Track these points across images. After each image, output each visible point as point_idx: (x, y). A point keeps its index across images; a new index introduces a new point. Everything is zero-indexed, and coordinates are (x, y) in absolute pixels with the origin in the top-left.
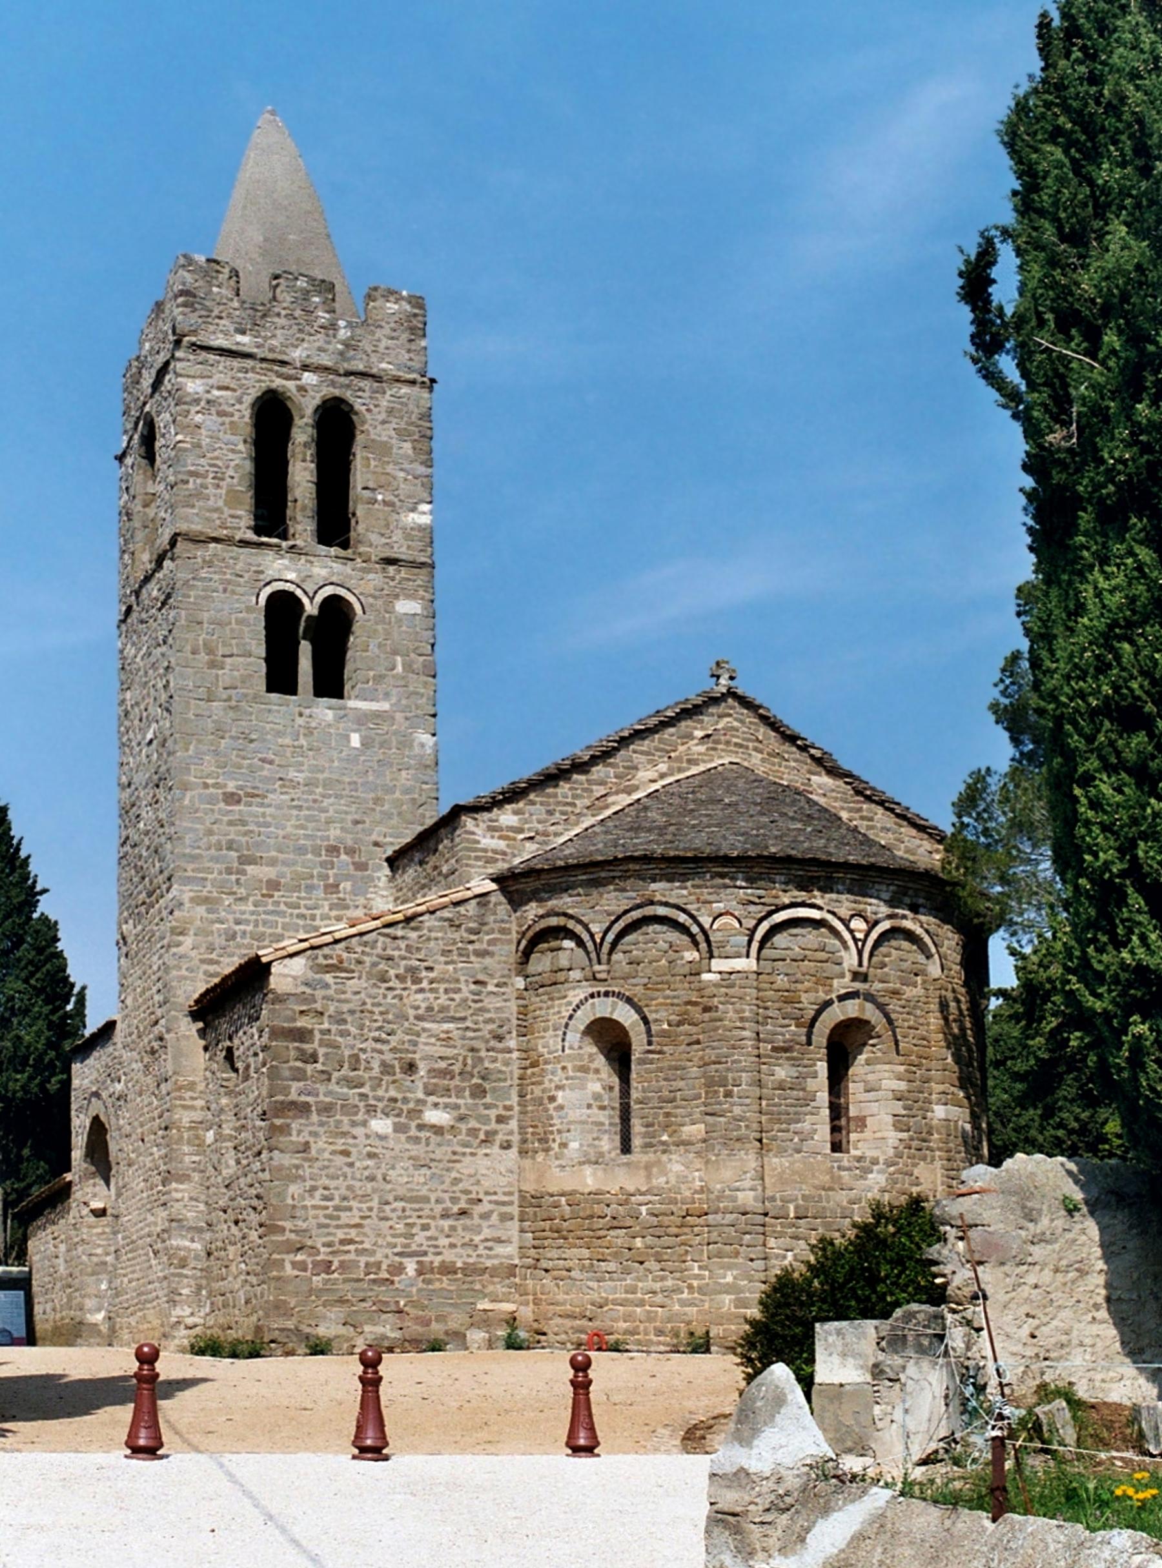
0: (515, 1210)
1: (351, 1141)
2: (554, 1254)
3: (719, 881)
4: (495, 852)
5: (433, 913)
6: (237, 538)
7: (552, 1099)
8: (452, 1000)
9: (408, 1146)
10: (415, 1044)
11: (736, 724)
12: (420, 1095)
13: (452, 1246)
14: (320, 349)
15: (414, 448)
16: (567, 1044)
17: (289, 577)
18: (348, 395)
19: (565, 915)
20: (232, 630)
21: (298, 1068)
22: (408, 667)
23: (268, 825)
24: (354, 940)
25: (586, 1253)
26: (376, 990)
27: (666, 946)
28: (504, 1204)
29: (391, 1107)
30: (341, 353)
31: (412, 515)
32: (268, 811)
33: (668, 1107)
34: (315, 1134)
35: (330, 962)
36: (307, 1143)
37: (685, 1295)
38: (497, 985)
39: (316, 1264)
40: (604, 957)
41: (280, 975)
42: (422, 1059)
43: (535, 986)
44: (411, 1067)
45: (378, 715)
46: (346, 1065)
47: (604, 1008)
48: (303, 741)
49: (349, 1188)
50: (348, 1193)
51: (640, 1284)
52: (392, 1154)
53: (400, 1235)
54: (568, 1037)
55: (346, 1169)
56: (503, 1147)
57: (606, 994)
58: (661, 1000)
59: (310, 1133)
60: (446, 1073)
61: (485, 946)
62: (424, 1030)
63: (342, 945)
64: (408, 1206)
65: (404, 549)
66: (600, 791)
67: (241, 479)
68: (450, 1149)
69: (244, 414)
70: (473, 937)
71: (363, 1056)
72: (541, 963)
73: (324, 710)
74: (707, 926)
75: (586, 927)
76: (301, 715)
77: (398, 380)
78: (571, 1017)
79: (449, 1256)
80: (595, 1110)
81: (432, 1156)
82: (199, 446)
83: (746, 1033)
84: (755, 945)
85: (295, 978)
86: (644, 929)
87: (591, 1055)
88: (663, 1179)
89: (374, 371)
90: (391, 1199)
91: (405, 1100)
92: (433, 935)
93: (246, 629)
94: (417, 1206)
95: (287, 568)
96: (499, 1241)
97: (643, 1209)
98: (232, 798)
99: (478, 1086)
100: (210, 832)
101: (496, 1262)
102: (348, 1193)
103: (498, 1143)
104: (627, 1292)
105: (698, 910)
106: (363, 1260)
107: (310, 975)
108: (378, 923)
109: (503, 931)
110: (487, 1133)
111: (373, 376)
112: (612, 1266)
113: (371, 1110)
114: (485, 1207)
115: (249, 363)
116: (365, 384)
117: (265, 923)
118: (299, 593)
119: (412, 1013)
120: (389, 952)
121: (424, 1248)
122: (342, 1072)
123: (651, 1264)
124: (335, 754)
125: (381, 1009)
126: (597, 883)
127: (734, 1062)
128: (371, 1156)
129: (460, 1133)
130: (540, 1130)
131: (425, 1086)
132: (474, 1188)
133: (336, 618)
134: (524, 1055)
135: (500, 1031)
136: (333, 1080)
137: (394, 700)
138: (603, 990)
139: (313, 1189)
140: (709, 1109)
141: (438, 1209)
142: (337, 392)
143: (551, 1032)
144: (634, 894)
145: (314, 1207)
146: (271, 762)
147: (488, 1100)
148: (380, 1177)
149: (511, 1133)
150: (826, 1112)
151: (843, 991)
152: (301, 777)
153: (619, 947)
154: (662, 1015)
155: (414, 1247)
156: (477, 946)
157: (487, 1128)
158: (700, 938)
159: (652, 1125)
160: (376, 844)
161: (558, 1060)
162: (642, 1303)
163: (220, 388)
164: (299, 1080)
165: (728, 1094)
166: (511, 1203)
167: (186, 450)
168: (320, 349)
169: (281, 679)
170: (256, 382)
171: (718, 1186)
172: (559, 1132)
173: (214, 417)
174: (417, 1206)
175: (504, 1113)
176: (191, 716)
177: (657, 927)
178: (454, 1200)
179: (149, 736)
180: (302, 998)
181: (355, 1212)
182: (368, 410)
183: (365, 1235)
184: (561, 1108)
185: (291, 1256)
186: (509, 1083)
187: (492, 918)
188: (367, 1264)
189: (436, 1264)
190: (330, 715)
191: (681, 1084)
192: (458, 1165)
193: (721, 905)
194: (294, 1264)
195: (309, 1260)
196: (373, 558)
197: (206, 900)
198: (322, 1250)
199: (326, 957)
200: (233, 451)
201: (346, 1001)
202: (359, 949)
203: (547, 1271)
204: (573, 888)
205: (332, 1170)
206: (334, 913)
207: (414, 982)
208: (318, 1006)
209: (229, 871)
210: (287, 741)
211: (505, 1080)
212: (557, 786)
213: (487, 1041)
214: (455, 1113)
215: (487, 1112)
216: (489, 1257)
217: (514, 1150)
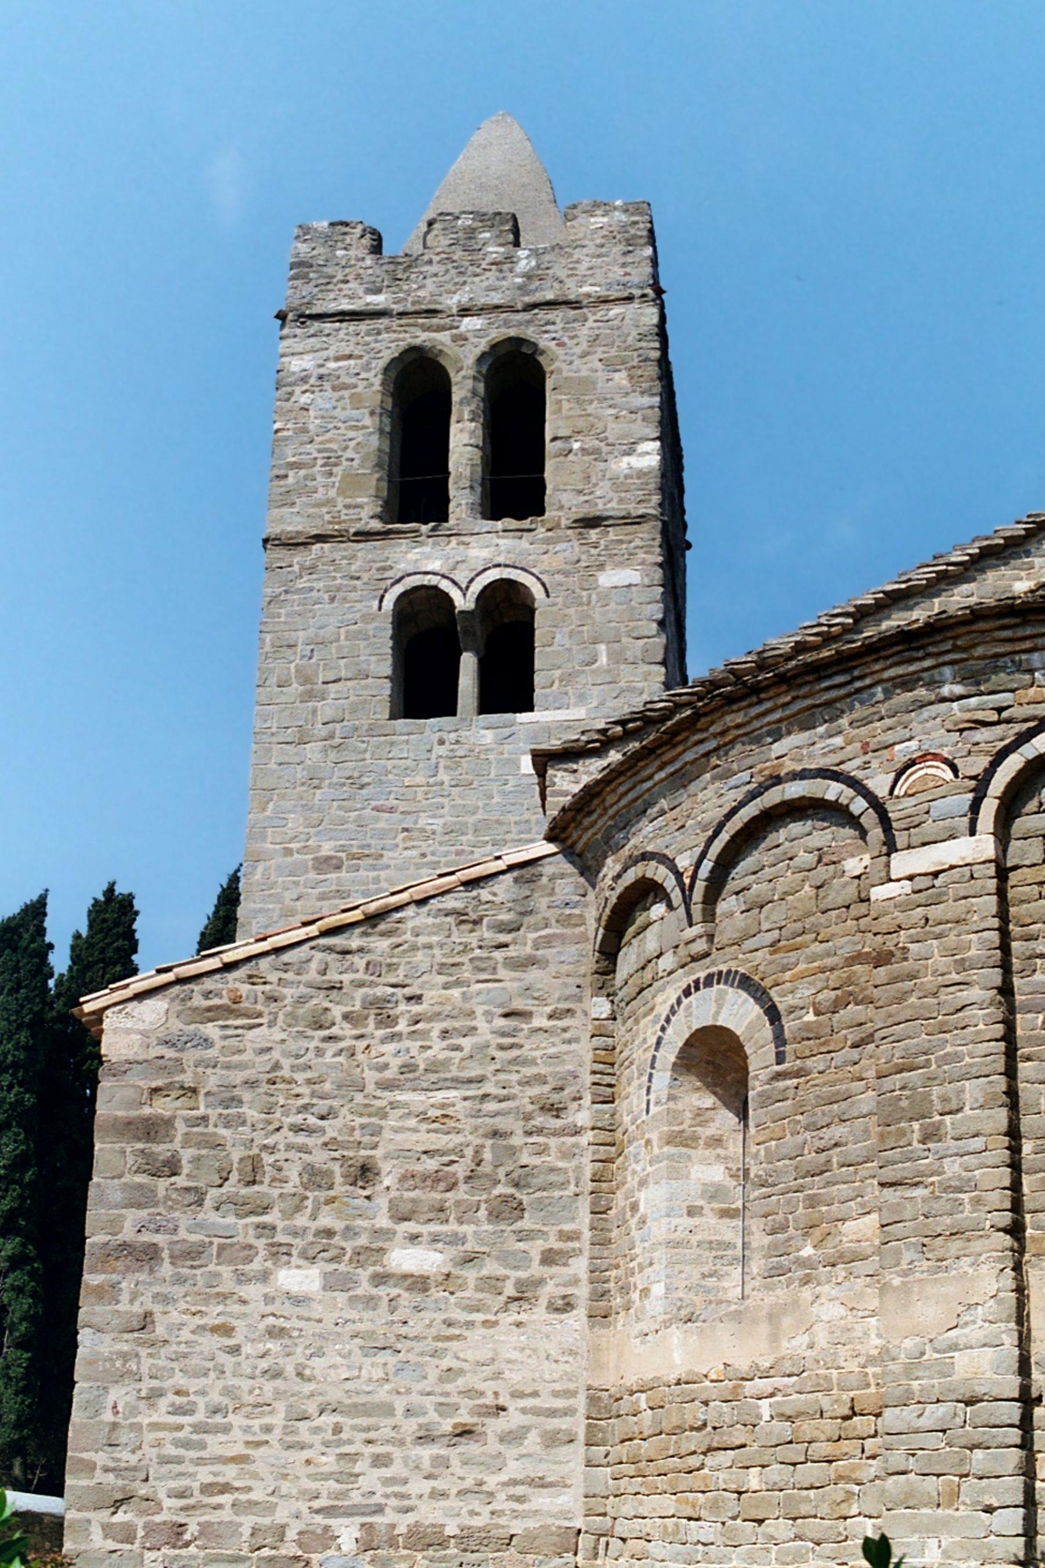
0: (578, 1425)
1: (237, 1308)
3: (905, 697)
5: (422, 902)
6: (352, 531)
8: (458, 1048)
9: (354, 1315)
10: (377, 1131)
12: (383, 1221)
13: (439, 1495)
14: (490, 289)
15: (631, 377)
17: (429, 568)
18: (530, 333)
20: (340, 648)
21: (141, 1186)
22: (618, 658)
24: (264, 963)
25: (668, 1504)
26: (304, 1044)
28: (553, 1413)
29: (322, 1246)
30: (520, 288)
31: (626, 459)
32: (383, 874)
33: (815, 1186)
34: (165, 1299)
35: (216, 1001)
36: (148, 1315)
39: (150, 1529)
40: (697, 916)
41: (115, 1030)
42: (386, 1157)
46: (234, 1177)
48: (443, 776)
49: (227, 1391)
50: (225, 1401)
52: (318, 1328)
53: (326, 1477)
55: (224, 1358)
56: (554, 1308)
57: (709, 981)
58: (802, 966)
59: (156, 1296)
61: (528, 950)
63: (242, 972)
65: (613, 504)
67: (363, 460)
68: (440, 1316)
69: (371, 384)
70: (503, 938)
71: (268, 1159)
76: (442, 742)
79: (428, 1514)
80: (709, 1220)
81: (404, 1330)
82: (305, 430)
84: (989, 807)
85: (144, 1034)
86: (772, 838)
87: (699, 1112)
88: (805, 1339)
89: (572, 297)
90: (312, 1408)
91: (349, 1232)
92: (422, 940)
93: (362, 644)
94: (364, 1421)
95: (428, 557)
97: (765, 1408)
98: (328, 864)
99: (505, 1199)
101: (531, 1524)
102: (225, 1401)
103: (543, 1302)
105: (865, 766)
106: (247, 1522)
107: (176, 1025)
108: (313, 930)
109: (564, 921)
110: (520, 1284)
111: (566, 303)
113: (279, 1253)
114: (513, 1419)
115: (382, 323)
116: (557, 315)
118: (445, 585)
119: (371, 1077)
120: (333, 976)
121: (377, 1499)
122: (227, 1188)
123: (781, 1528)
124: (494, 787)
125: (309, 1074)
127: (946, 1059)
128: (273, 1333)
129: (462, 1287)
131: (392, 1205)
132: (489, 1387)
134: (605, 1137)
135: (555, 1097)
136: (208, 1203)
138: (702, 975)
139: (154, 1395)
140: (889, 1174)
141: (410, 1427)
142: (512, 332)
144: (745, 776)
145: (155, 1426)
146: (392, 810)
147: (527, 1223)
148: (290, 1370)
149: (575, 1282)
152: (438, 824)
155: (356, 1498)
156: (512, 952)
157: (522, 1274)
158: (870, 819)
159: (784, 1228)
163: (337, 359)
164: (139, 1206)
167: (286, 438)
170: (391, 342)
171: (908, 1343)
173: (329, 393)
174: (364, 1421)
175: (557, 1245)
176: (272, 766)
177: (796, 828)
178: (443, 1409)
180: (159, 1065)
181: (236, 1434)
182: (561, 344)
183: (255, 1476)
185: (104, 1515)
187: (544, 902)
189: (402, 1529)
191: (838, 1131)
192: (454, 1345)
193: (913, 744)
194: (108, 1530)
195: (140, 1522)
196: (564, 522)
198: (167, 1502)
200: (355, 428)
201: (241, 1066)
202: (273, 977)
204: (651, 804)
205: (194, 1361)
207: (379, 1024)
208: (187, 1078)
210: (420, 779)
211: (563, 1185)
213: (528, 1117)
214: (454, 1251)
216: (516, 1515)
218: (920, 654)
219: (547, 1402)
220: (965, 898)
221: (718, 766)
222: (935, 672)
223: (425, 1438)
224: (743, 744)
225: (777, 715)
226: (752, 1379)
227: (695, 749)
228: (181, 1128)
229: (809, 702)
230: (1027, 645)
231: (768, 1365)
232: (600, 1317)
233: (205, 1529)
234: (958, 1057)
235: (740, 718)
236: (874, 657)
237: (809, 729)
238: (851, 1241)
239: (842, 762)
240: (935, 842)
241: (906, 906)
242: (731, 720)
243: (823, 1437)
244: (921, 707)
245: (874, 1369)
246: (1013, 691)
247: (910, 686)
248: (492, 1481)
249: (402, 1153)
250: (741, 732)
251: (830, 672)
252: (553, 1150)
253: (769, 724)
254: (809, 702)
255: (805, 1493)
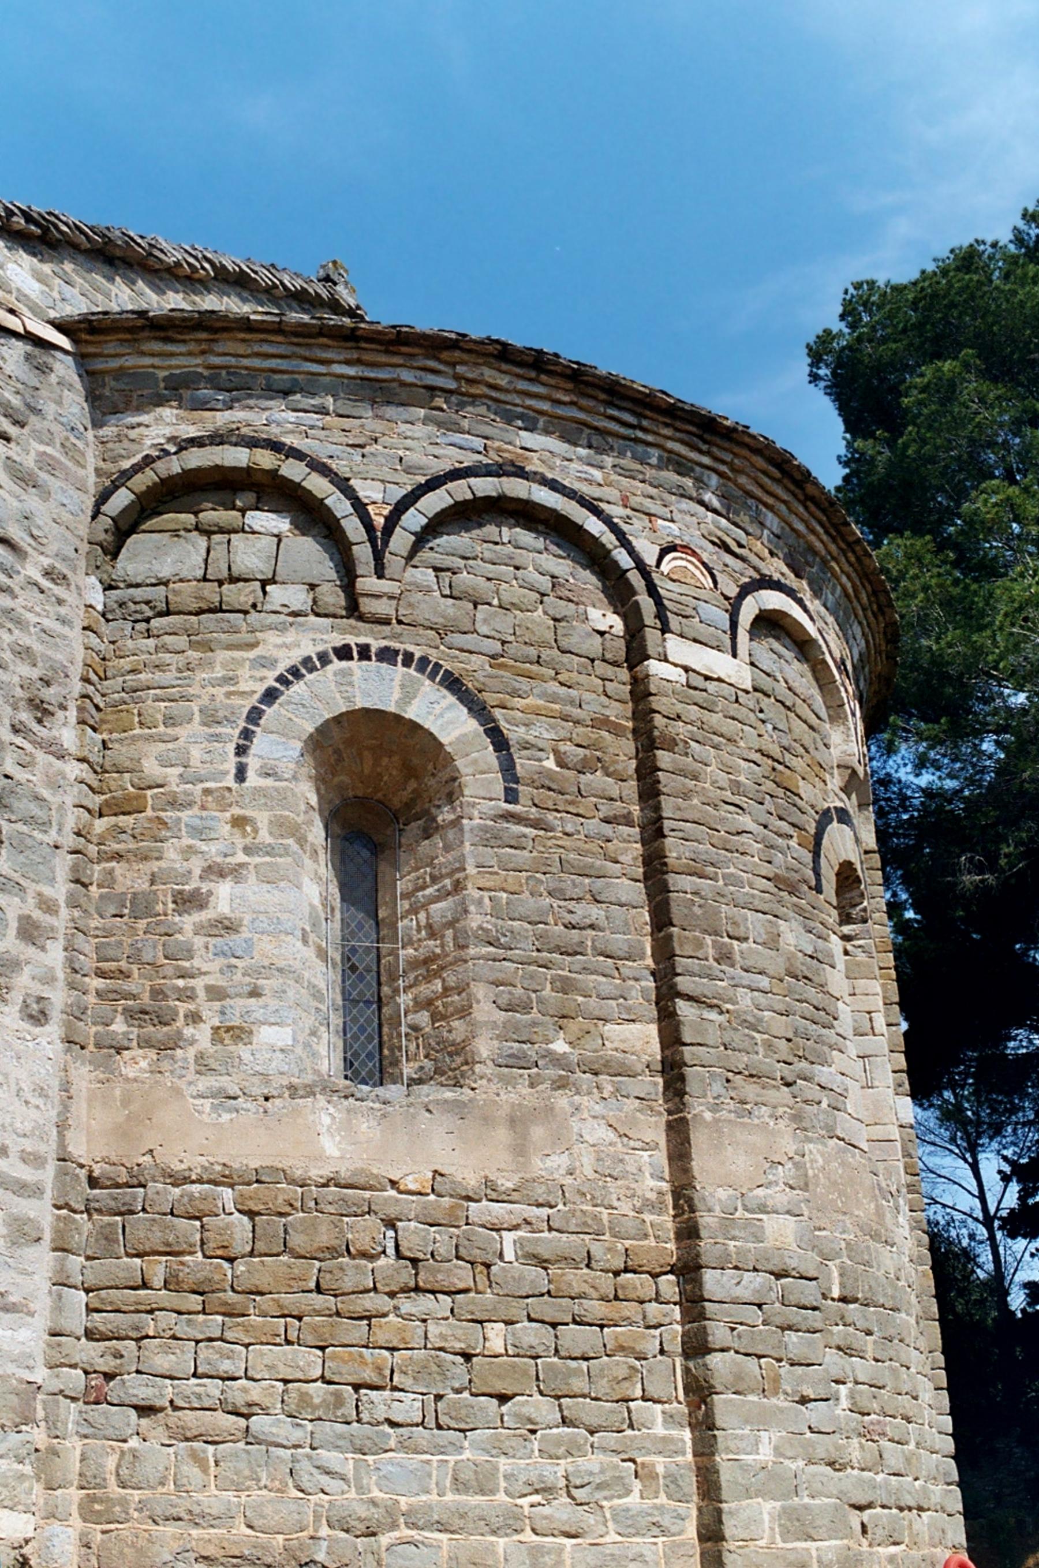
2: (181, 1359)
3: (670, 476)
16: (252, 762)
19: (275, 446)
25: (310, 1361)
27: (545, 583)
37: (633, 1500)
38: (47, 574)
40: (393, 563)
43: (143, 610)
47: (377, 687)
51: (504, 1464)
54: (260, 744)
57: (387, 655)
72: (167, 555)
74: (650, 560)
75: (344, 486)
78: (270, 696)
83: (745, 821)
86: (490, 530)
103: (17, 997)
104: (459, 1485)
105: (627, 519)
112: (408, 1407)
123: (543, 1409)
126: (380, 394)
130: (138, 984)
138: (375, 645)
143: (195, 726)
153: (425, 555)
154: (542, 732)
159: (526, 1007)
161: (221, 799)
162: (509, 1524)
165: (724, 957)
166: (34, 1191)
172: (216, 993)
184: (227, 926)
186: (52, 837)
203: (145, 1410)
211: (45, 825)
212: (111, 280)
217: (53, 1030)
218: (705, 447)
220: (734, 719)
221: (442, 410)
222: (707, 472)
224: (489, 408)
225: (545, 406)
226: (478, 1201)
227: (419, 373)
229: (581, 416)
230: (770, 501)
231: (510, 1185)
234: (739, 883)
235: (503, 381)
236: (668, 421)
237: (569, 442)
238: (616, 1050)
239: (601, 500)
240: (706, 645)
242: (489, 374)
243: (595, 1295)
244: (682, 496)
245: (653, 1217)
246: (748, 534)
247: (682, 470)
250: (494, 394)
251: (624, 404)
252: (39, 769)
253: (529, 408)
254: (581, 416)
255: (573, 1364)
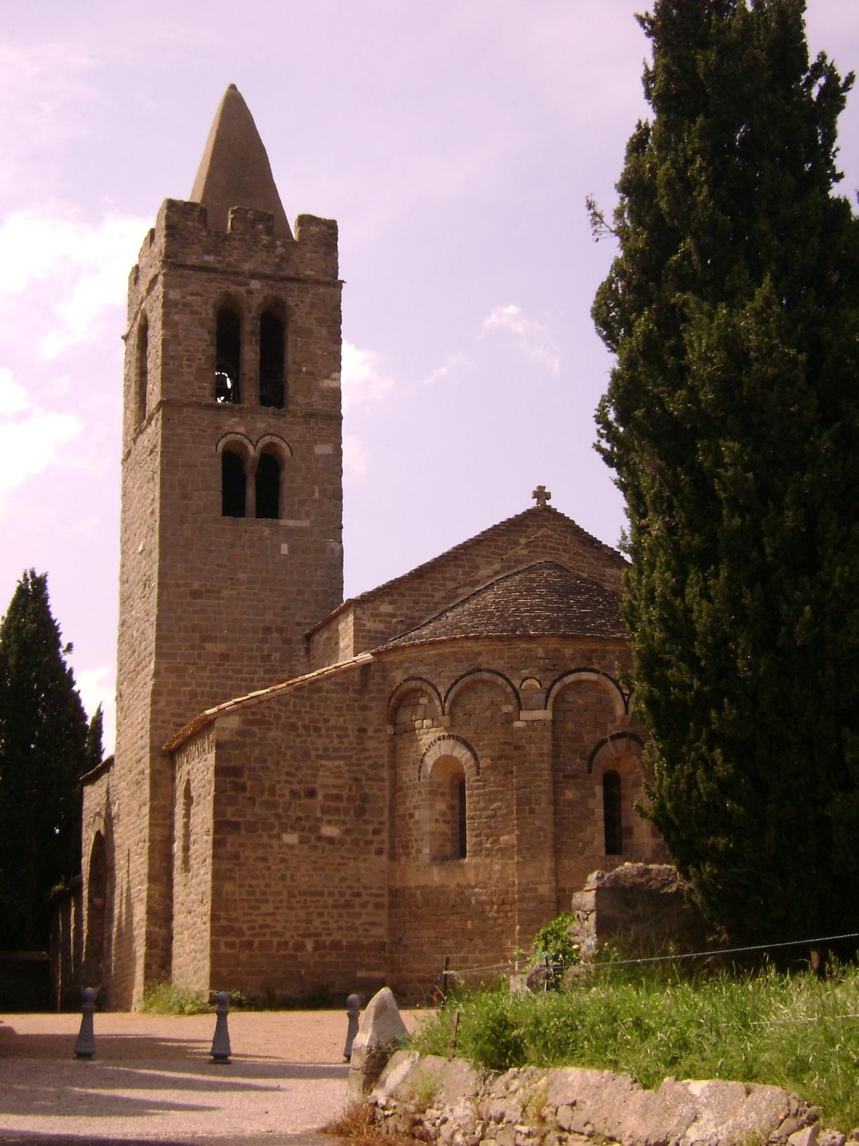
0: (385, 900)
4: (376, 632)
7: (412, 816)
10: (315, 776)
11: (550, 533)
13: (340, 928)
14: (264, 262)
19: (421, 679)
23: (220, 612)
28: (376, 896)
39: (242, 943)
44: (312, 794)
45: (301, 530)
60: (338, 798)
62: (322, 766)
64: (309, 899)
66: (450, 585)
71: (278, 786)
73: (264, 528)
74: (517, 687)
77: (317, 282)
79: (337, 936)
90: (296, 892)
95: (238, 424)
96: (373, 924)
98: (196, 594)
100: (179, 619)
101: (371, 940)
106: (275, 940)
113: (284, 828)
115: (213, 276)
117: (218, 685)
118: (246, 441)
128: (283, 861)
133: (271, 464)
137: (312, 518)
141: (330, 901)
149: (383, 842)
150: (601, 824)
151: (614, 733)
155: (312, 930)
158: (512, 696)
160: (298, 624)
163: (192, 294)
165: (532, 811)
166: (382, 895)
168: (264, 262)
169: (233, 506)
178: (342, 894)
179: (141, 548)
184: (417, 822)
188: (279, 944)
190: (267, 532)
197: (176, 670)
198: (248, 932)
199: (253, 714)
206: (267, 677)
209: (193, 647)
215: (364, 827)
216: (366, 937)
219: (374, 891)
223: (335, 907)
228: (246, 772)
232: (393, 857)
233: (261, 943)
241: (524, 730)
248: (358, 923)
249: (322, 786)
